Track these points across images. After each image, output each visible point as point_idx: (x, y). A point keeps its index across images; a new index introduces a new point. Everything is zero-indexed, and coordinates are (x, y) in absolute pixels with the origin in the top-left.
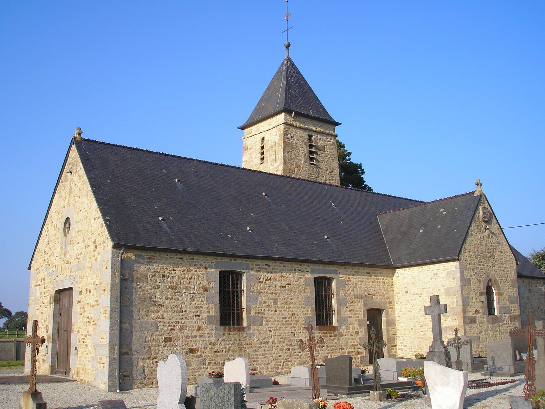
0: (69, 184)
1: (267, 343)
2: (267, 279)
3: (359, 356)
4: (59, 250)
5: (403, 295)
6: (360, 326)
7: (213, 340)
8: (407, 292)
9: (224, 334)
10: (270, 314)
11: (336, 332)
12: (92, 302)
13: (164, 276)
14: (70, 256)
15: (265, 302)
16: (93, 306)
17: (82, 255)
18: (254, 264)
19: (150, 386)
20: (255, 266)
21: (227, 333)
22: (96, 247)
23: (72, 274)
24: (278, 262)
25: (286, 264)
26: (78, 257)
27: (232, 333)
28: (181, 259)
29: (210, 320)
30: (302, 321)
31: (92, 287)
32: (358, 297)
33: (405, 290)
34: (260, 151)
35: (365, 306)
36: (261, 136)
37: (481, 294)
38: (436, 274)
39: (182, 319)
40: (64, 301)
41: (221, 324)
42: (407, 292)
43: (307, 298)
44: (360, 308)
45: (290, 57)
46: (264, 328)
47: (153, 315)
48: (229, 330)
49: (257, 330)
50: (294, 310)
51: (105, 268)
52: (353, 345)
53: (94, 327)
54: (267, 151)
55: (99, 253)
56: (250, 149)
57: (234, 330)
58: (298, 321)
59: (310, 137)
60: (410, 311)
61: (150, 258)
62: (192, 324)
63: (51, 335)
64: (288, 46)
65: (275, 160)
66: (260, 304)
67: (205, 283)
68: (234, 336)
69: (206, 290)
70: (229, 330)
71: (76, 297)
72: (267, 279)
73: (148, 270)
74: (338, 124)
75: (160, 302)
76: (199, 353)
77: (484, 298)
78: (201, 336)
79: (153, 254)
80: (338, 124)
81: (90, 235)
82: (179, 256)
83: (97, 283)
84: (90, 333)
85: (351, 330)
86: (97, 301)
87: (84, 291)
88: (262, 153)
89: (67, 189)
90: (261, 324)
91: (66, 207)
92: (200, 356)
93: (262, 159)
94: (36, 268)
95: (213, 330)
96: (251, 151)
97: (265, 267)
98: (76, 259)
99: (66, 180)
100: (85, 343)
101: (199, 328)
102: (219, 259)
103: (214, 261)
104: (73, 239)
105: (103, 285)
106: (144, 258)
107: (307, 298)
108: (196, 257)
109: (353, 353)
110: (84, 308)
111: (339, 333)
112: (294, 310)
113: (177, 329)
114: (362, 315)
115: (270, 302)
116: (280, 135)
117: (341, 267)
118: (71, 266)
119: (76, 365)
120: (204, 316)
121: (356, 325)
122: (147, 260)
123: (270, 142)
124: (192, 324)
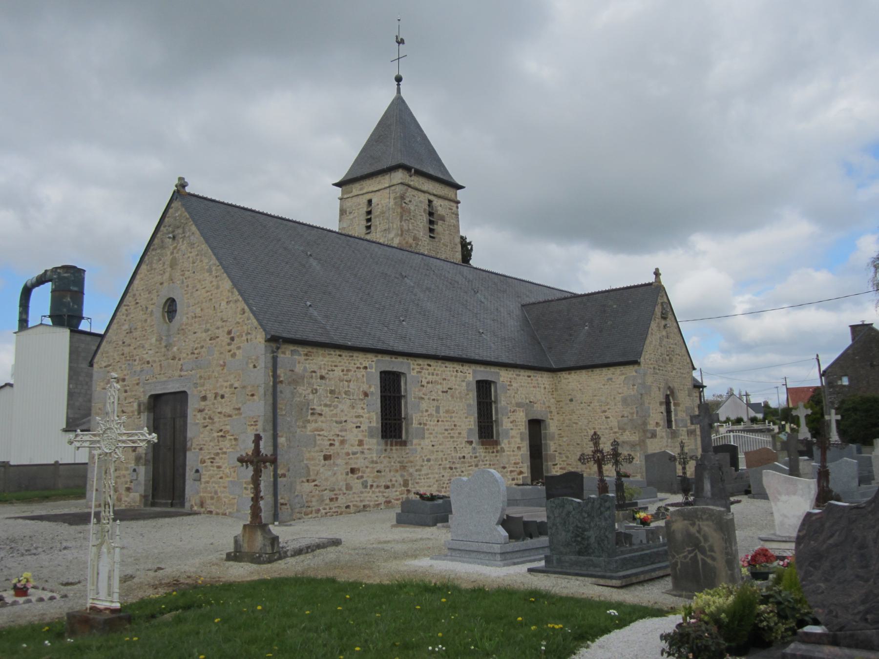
0: (169, 253)
1: (429, 460)
2: (428, 383)
3: (521, 476)
4: (154, 340)
5: (567, 404)
6: (522, 439)
7: (375, 456)
8: (571, 400)
9: (386, 450)
10: (431, 424)
11: (499, 448)
12: (227, 410)
13: (322, 378)
14: (178, 349)
15: (427, 411)
16: (230, 416)
17: (204, 349)
18: (416, 363)
19: (314, 515)
20: (416, 367)
21: (389, 447)
22: (232, 339)
23: (183, 373)
24: (440, 362)
25: (447, 364)
26: (196, 352)
27: (394, 448)
28: (340, 356)
29: (371, 433)
30: (465, 434)
31: (227, 391)
32: (519, 405)
33: (570, 397)
34: (364, 217)
35: (526, 415)
36: (368, 197)
37: (661, 404)
38: (611, 379)
39: (341, 431)
40: (167, 410)
41: (383, 437)
42: (571, 400)
43: (469, 405)
44: (521, 418)
45: (402, 94)
46: (427, 441)
47: (310, 427)
48: (391, 445)
49: (420, 445)
50: (456, 420)
51: (251, 366)
52: (515, 463)
53: (234, 443)
54: (375, 218)
55: (239, 348)
56: (350, 213)
57: (396, 445)
58: (460, 433)
59: (430, 201)
60: (576, 423)
61: (306, 355)
62: (353, 436)
63: (143, 456)
64: (399, 79)
65: (387, 230)
66: (422, 412)
67: (365, 387)
68: (396, 452)
69: (366, 395)
70: (391, 445)
71: (193, 404)
72: (428, 383)
73: (305, 369)
74: (460, 187)
75: (318, 409)
76: (360, 474)
77: (663, 408)
78: (363, 453)
79: (309, 349)
80: (460, 187)
81: (219, 323)
82: (338, 353)
83: (236, 385)
84: (224, 450)
85: (512, 445)
86: (239, 409)
87: (210, 396)
88: (369, 220)
89: (168, 258)
90: (423, 438)
91: (165, 284)
92: (362, 477)
93: (368, 227)
94: (104, 364)
95: (374, 444)
96: (351, 216)
97: (426, 367)
98: (193, 353)
99: (162, 247)
100: (215, 464)
101: (361, 443)
102: (380, 357)
103: (375, 359)
104: (184, 327)
105: (249, 388)
106: (300, 355)
107: (469, 405)
108: (355, 354)
109: (515, 473)
110: (210, 418)
111: (502, 448)
112: (456, 420)
113: (337, 443)
114: (523, 428)
115: (432, 411)
116: (395, 198)
117: (503, 369)
118: (180, 362)
119: (198, 492)
120: (364, 427)
121: (518, 440)
122: (303, 358)
123: (380, 206)
124: (353, 436)
